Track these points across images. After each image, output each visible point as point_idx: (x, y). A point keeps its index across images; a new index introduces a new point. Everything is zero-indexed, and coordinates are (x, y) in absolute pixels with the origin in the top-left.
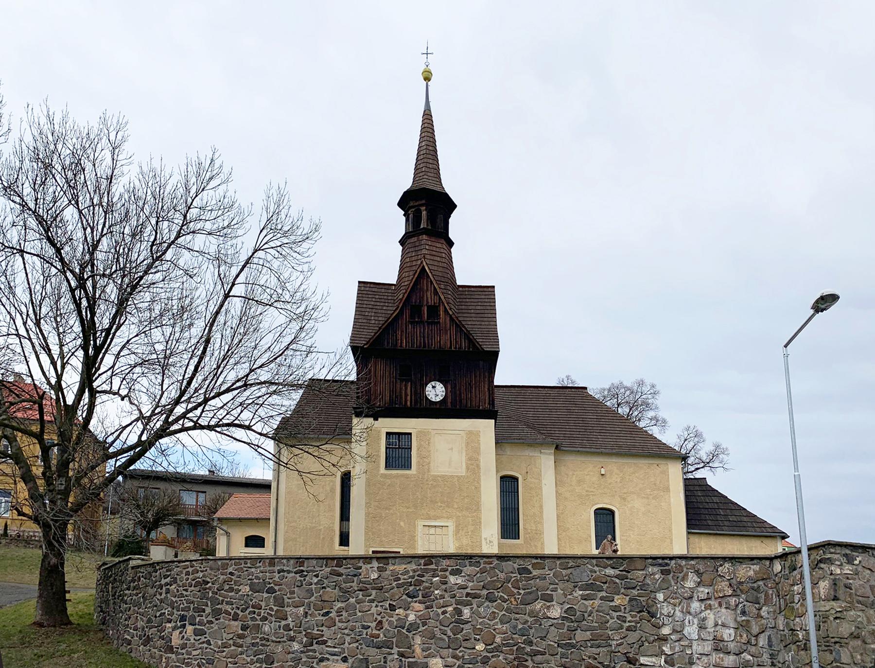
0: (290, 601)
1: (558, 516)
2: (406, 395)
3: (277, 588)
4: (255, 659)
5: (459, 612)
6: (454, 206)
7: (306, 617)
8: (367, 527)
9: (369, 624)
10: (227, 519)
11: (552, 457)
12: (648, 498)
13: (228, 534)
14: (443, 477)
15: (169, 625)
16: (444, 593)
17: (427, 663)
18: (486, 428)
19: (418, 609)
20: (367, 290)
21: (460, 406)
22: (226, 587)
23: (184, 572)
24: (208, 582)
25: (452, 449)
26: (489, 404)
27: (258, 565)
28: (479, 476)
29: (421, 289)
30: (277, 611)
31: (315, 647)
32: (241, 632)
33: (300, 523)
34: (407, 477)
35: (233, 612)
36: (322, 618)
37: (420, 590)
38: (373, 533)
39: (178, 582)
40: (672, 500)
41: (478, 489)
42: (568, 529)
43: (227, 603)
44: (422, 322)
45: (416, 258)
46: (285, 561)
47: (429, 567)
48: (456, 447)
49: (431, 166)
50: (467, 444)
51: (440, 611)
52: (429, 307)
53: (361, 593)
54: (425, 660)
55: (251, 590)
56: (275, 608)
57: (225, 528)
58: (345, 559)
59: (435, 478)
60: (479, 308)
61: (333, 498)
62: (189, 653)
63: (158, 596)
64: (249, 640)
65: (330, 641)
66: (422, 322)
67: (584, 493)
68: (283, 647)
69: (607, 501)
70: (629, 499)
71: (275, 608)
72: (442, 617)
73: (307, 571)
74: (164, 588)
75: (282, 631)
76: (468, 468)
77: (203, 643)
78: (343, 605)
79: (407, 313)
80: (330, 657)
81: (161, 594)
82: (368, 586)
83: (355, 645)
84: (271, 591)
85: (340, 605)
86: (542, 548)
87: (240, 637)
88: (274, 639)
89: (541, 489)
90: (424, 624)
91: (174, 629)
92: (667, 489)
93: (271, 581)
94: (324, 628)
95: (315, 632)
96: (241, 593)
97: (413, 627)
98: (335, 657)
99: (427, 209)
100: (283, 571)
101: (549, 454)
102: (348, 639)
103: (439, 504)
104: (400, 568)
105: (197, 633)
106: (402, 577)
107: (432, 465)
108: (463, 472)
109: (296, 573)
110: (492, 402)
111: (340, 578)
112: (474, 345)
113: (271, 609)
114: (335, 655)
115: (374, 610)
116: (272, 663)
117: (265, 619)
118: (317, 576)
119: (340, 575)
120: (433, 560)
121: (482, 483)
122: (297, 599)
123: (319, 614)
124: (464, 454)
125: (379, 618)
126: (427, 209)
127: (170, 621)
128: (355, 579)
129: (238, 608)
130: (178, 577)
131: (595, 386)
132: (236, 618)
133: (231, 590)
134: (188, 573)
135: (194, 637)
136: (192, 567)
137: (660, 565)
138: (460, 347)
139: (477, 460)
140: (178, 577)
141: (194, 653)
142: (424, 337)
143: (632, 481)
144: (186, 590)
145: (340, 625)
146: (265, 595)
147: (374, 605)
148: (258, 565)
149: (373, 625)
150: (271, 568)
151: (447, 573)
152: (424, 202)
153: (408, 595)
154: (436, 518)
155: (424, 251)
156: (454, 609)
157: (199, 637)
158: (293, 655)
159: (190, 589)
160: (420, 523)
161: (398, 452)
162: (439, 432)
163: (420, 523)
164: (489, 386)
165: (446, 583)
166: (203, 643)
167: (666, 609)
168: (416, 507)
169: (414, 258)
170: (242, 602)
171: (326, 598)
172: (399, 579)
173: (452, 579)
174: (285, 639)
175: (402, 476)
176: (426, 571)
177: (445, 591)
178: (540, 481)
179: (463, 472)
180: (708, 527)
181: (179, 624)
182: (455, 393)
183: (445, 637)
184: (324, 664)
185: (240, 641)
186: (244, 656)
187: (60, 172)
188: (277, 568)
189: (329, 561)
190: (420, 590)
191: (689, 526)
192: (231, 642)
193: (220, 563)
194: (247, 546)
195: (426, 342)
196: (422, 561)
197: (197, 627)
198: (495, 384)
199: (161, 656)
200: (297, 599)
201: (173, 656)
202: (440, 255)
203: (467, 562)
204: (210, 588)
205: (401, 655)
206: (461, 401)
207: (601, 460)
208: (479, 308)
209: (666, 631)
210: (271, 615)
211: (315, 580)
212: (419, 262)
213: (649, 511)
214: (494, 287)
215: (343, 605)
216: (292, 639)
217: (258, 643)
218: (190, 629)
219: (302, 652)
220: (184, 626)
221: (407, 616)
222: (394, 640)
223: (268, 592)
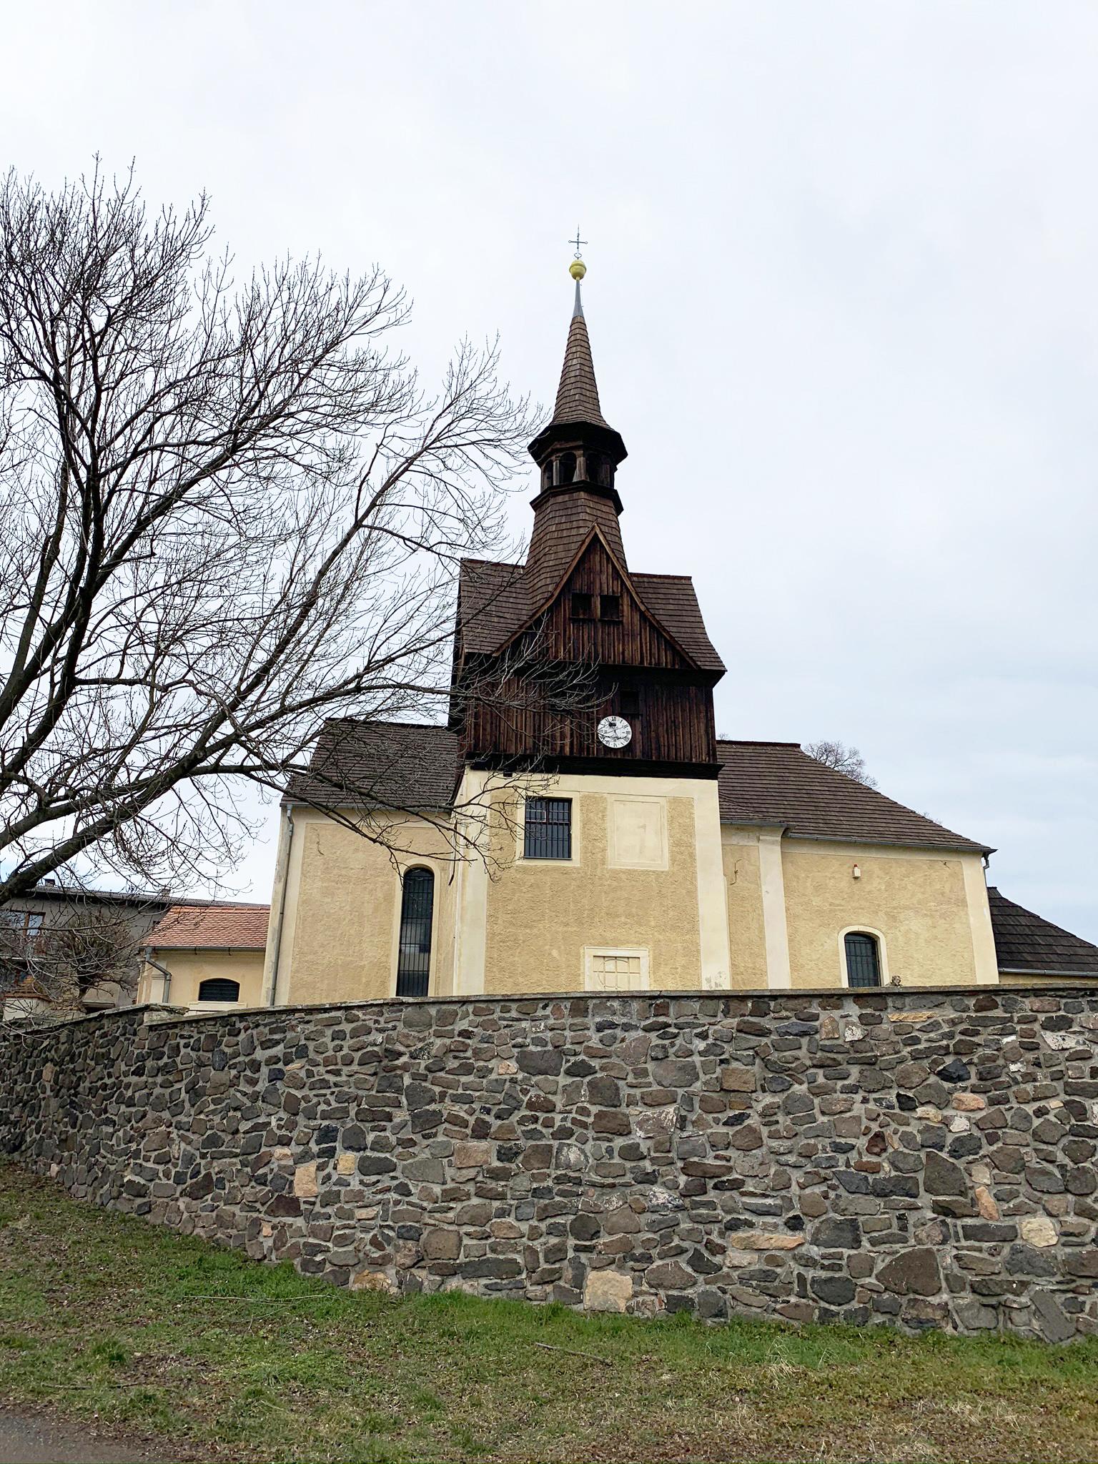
0: (637, 1092)
1: (790, 941)
3: (595, 1063)
4: (543, 1226)
6: (623, 454)
7: (682, 1129)
8: (489, 959)
9: (852, 1141)
11: (779, 848)
12: (932, 916)
13: (166, 976)
14: (629, 872)
15: (279, 1151)
16: (1032, 1069)
17: (1014, 1227)
18: (703, 795)
19: (973, 1105)
20: (474, 573)
21: (659, 756)
22: (452, 1064)
23: (329, 1032)
24: (401, 1054)
25: (644, 827)
26: (708, 754)
27: (540, 1013)
28: (694, 873)
29: (591, 570)
30: (599, 1116)
31: (712, 1195)
32: (499, 1164)
33: (335, 954)
34: (565, 872)
35: (472, 1120)
36: (724, 1130)
37: (970, 1063)
38: (502, 970)
39: (312, 1055)
40: (972, 919)
41: (692, 894)
42: (803, 966)
43: (456, 1099)
44: (591, 620)
45: (568, 525)
46: (616, 1004)
47: (990, 1014)
48: (638, 821)
49: (588, 394)
50: (672, 820)
51: (1030, 1109)
52: (604, 599)
53: (820, 1072)
54: (1008, 1222)
55: (521, 1069)
56: (594, 1109)
57: (163, 965)
58: (774, 998)
59: (615, 875)
60: (672, 607)
61: (389, 912)
62: (345, 1215)
63: (244, 1087)
64: (523, 1183)
65: (750, 1182)
66: (591, 620)
67: (827, 907)
68: (624, 1197)
69: (866, 921)
70: (902, 917)
71: (594, 1109)
72: (1037, 1122)
73: (676, 1026)
74: (265, 1070)
75: (617, 1160)
76: (673, 860)
77: (388, 1190)
78: (777, 1099)
79: (567, 607)
80: (754, 1219)
81: (253, 1082)
82: (839, 1057)
83: (818, 1190)
84: (579, 1070)
85: (768, 1099)
87: (495, 1175)
88: (598, 1179)
89: (760, 898)
90: (992, 1139)
91: (302, 1158)
92: (962, 903)
93: (578, 1048)
94: (730, 1153)
95: (710, 1161)
96: (493, 1076)
97: (963, 1147)
98: (769, 1219)
100: (612, 1025)
101: (773, 843)
102: (797, 1176)
103: (623, 919)
104: (916, 1017)
105: (365, 1167)
106: (924, 1037)
107: (609, 853)
108: (664, 864)
109: (646, 1030)
110: (712, 752)
111: (764, 1040)
112: (683, 660)
113: (584, 1111)
114: (768, 1214)
115: (858, 1109)
116: (596, 1234)
117: (564, 1133)
118: (703, 1036)
119: (764, 1033)
120: (998, 999)
121: (700, 883)
122: (655, 1087)
123: (717, 1121)
124: (666, 833)
125: (875, 1128)
126: (579, 454)
127: (285, 1142)
128: (805, 1041)
129: (488, 1111)
130: (311, 1045)
131: (809, 743)
132: (481, 1132)
133: (467, 1069)
134: (339, 1036)
135: (358, 1177)
136: (349, 1021)
138: (659, 663)
139: (691, 845)
140: (311, 1045)
141: (362, 1214)
142: (595, 644)
143: (905, 888)
144: (337, 1073)
145: (774, 1143)
146: (563, 1080)
147: (858, 1097)
148: (540, 1013)
149: (862, 1142)
150: (578, 1020)
151: (1036, 1027)
152: (581, 443)
153: (945, 1075)
154: (616, 943)
155: (582, 516)
156: (1066, 1104)
157: (374, 1178)
158: (655, 1216)
159: (345, 1070)
160: (588, 952)
161: (549, 830)
162: (623, 798)
163: (588, 952)
164: (707, 727)
165: (1034, 1047)
166: (388, 1190)
168: (580, 922)
169: (564, 526)
170: (500, 1097)
171: (731, 1084)
172: (916, 1041)
173: (1052, 1040)
174: (628, 1178)
175: (555, 869)
176: (985, 1022)
177: (1038, 1065)
178: (759, 886)
179: (664, 864)
180: (1027, 964)
181: (315, 1148)
182: (649, 738)
183: (1050, 1167)
184: (741, 1234)
185: (499, 1186)
186: (511, 1220)
187: (50, 284)
188: (593, 1021)
189: (734, 1004)
190: (970, 1063)
191: (1000, 964)
192: (471, 1188)
193: (433, 1011)
194: (202, 997)
196: (971, 1002)
197: (369, 1153)
199: (256, 1223)
200: (655, 1087)
201: (299, 1222)
203: (1084, 1001)
204: (405, 1068)
205: (944, 1210)
206: (658, 749)
207: (874, 855)
208: (672, 607)
210: (585, 1125)
211: (702, 1045)
212: (590, 524)
213: (936, 938)
214: (690, 578)
215: (777, 1099)
216: (650, 1179)
217: (549, 1190)
218: (347, 1160)
219: (679, 1208)
220: (331, 1153)
221: (946, 1122)
222: (921, 1176)
223: (569, 1073)
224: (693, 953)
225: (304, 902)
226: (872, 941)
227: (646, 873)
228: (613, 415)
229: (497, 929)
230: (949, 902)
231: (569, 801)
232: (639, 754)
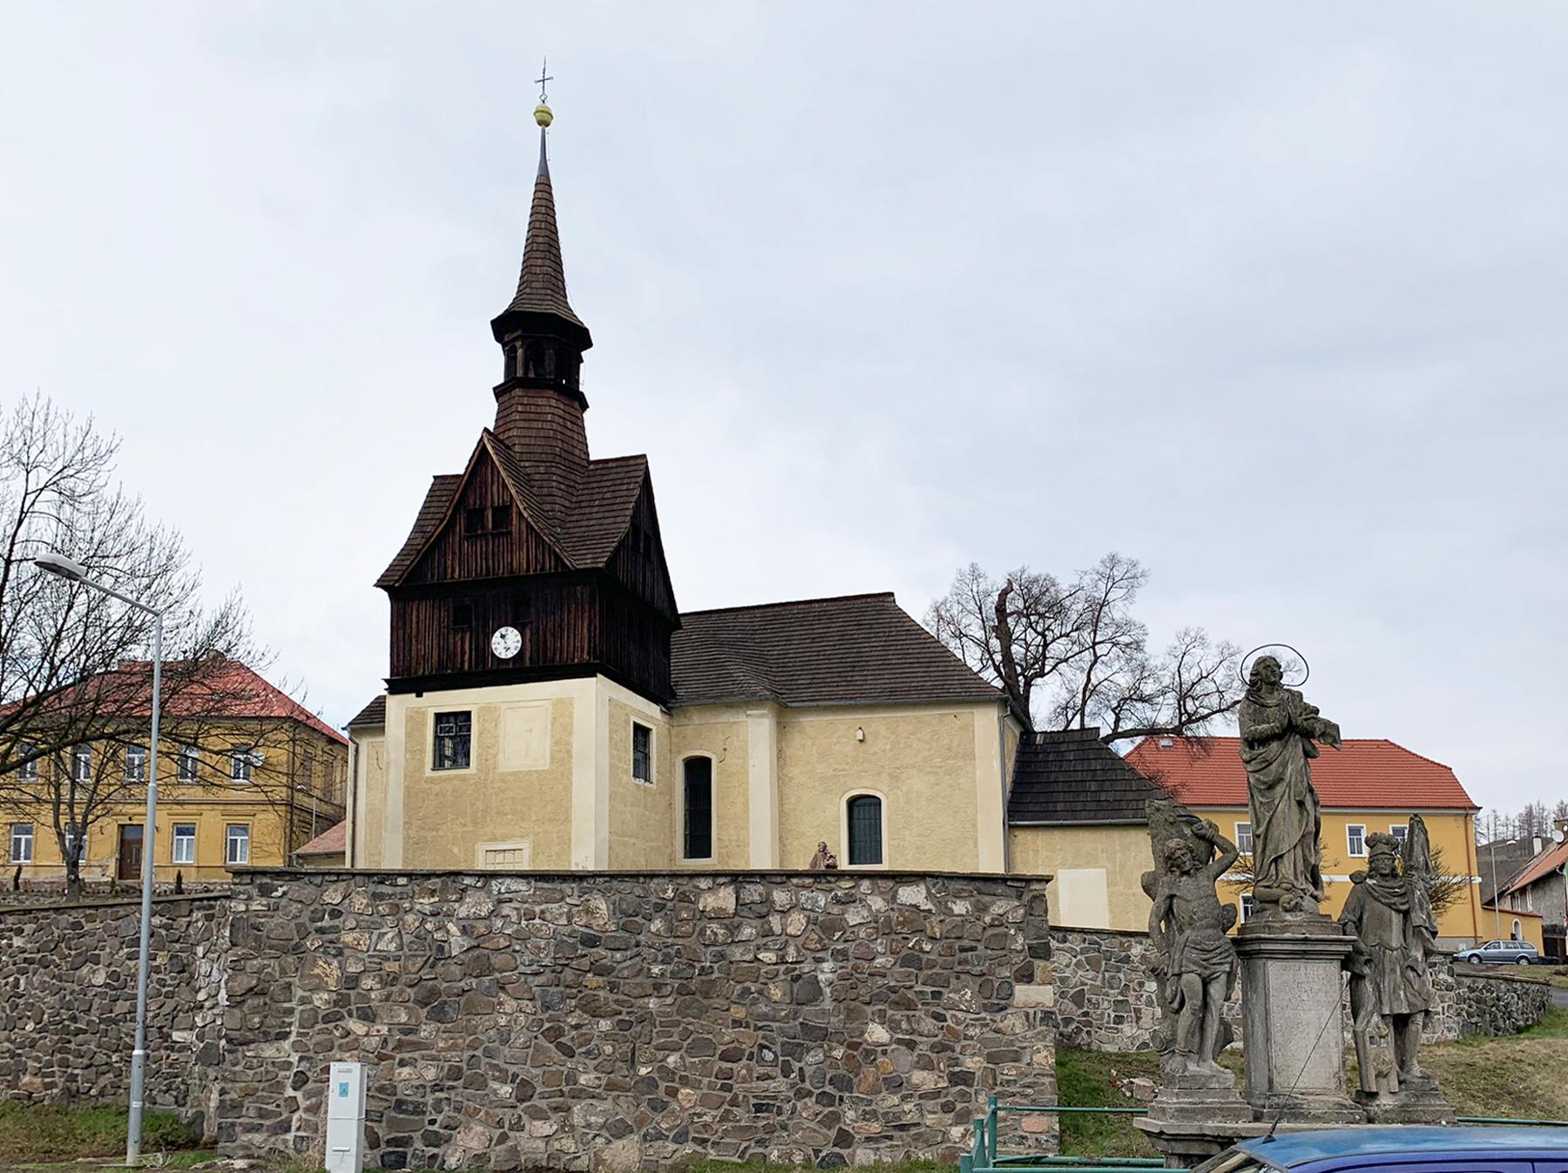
2: (463, 654)
5: (16, 984)
10: (312, 855)
12: (936, 773)
34: (463, 779)
41: (568, 789)
44: (484, 535)
52: (494, 509)
59: (504, 778)
76: (553, 758)
79: (460, 527)
86: (747, 862)
99: (542, 344)
101: (761, 716)
107: (500, 756)
108: (544, 764)
121: (574, 778)
126: (542, 344)
137: (204, 908)
139: (569, 743)
167: (204, 967)
168: (475, 823)
175: (456, 777)
178: (746, 760)
179: (544, 764)
195: (531, 560)
198: (680, 611)
202: (543, 417)
209: (201, 996)
214: (644, 456)
224: (565, 842)
225: (370, 812)
226: (874, 802)
227: (529, 773)
228: (582, 304)
229: (412, 833)
230: (955, 757)
231: (468, 714)
232: (528, 663)
